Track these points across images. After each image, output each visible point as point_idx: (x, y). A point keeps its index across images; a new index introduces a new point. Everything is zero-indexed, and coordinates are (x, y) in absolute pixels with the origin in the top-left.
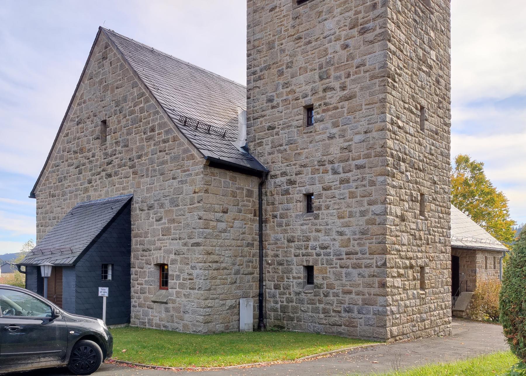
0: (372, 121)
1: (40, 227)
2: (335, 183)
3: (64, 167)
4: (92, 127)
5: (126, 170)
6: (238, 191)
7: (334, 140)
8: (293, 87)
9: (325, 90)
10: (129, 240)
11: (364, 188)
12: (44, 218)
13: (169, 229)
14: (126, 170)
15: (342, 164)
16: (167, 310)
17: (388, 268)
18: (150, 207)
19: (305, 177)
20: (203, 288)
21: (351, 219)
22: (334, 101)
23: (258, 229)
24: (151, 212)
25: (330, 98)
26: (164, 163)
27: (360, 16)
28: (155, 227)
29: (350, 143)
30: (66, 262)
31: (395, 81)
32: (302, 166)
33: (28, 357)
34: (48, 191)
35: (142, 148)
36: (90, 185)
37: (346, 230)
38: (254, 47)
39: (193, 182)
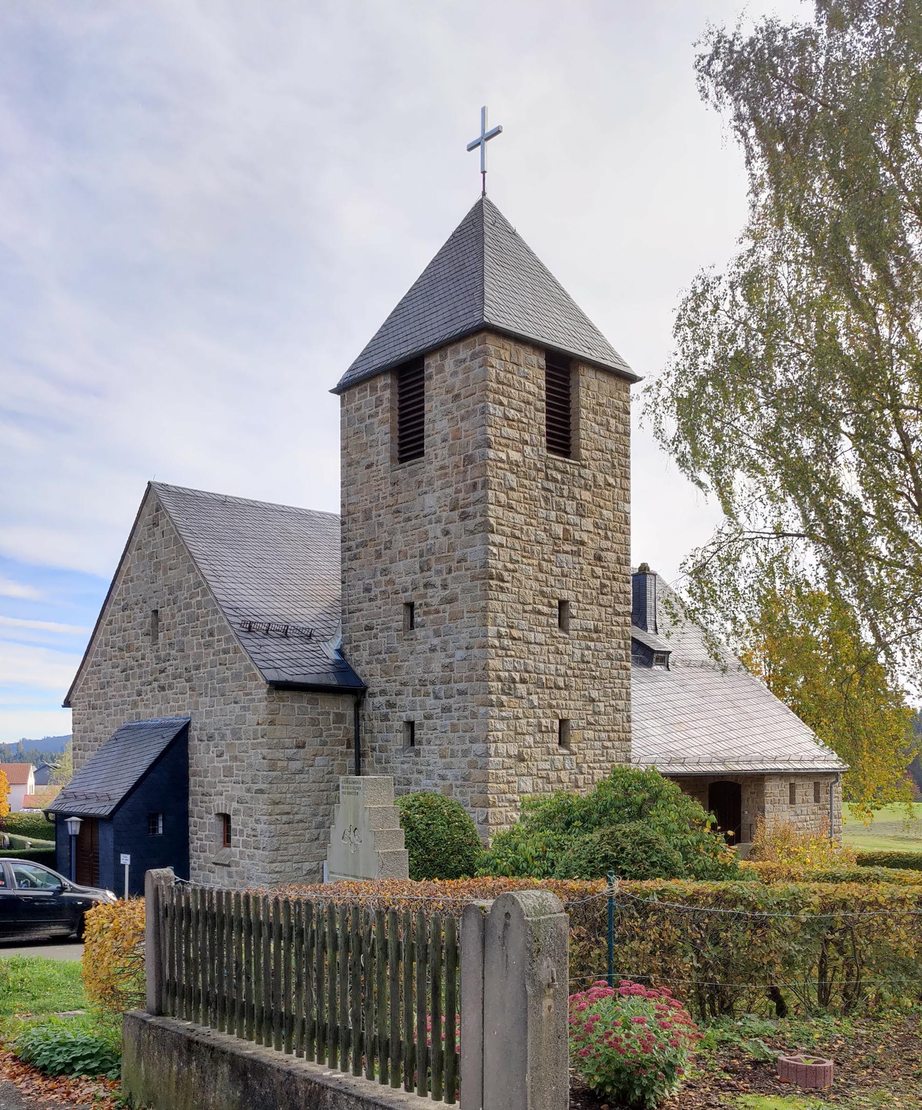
0: (474, 635)
1: (77, 751)
2: (436, 711)
3: (106, 668)
4: (140, 616)
5: (181, 684)
6: (321, 717)
7: (436, 653)
8: (392, 576)
9: (426, 586)
10: (187, 780)
11: (466, 721)
12: (82, 738)
13: (231, 768)
14: (181, 684)
15: (443, 687)
16: (230, 875)
17: (492, 825)
18: (211, 738)
19: (405, 700)
20: (268, 848)
21: (453, 760)
22: (435, 601)
23: (353, 765)
24: (211, 743)
25: (431, 597)
26: (224, 680)
27: (461, 495)
28: (215, 764)
29: (452, 660)
30: (102, 813)
31: (503, 581)
32: (402, 684)
33: (38, 925)
34: (86, 699)
35: (199, 656)
36: (139, 698)
37: (449, 773)
38: (349, 513)
39: (256, 709)
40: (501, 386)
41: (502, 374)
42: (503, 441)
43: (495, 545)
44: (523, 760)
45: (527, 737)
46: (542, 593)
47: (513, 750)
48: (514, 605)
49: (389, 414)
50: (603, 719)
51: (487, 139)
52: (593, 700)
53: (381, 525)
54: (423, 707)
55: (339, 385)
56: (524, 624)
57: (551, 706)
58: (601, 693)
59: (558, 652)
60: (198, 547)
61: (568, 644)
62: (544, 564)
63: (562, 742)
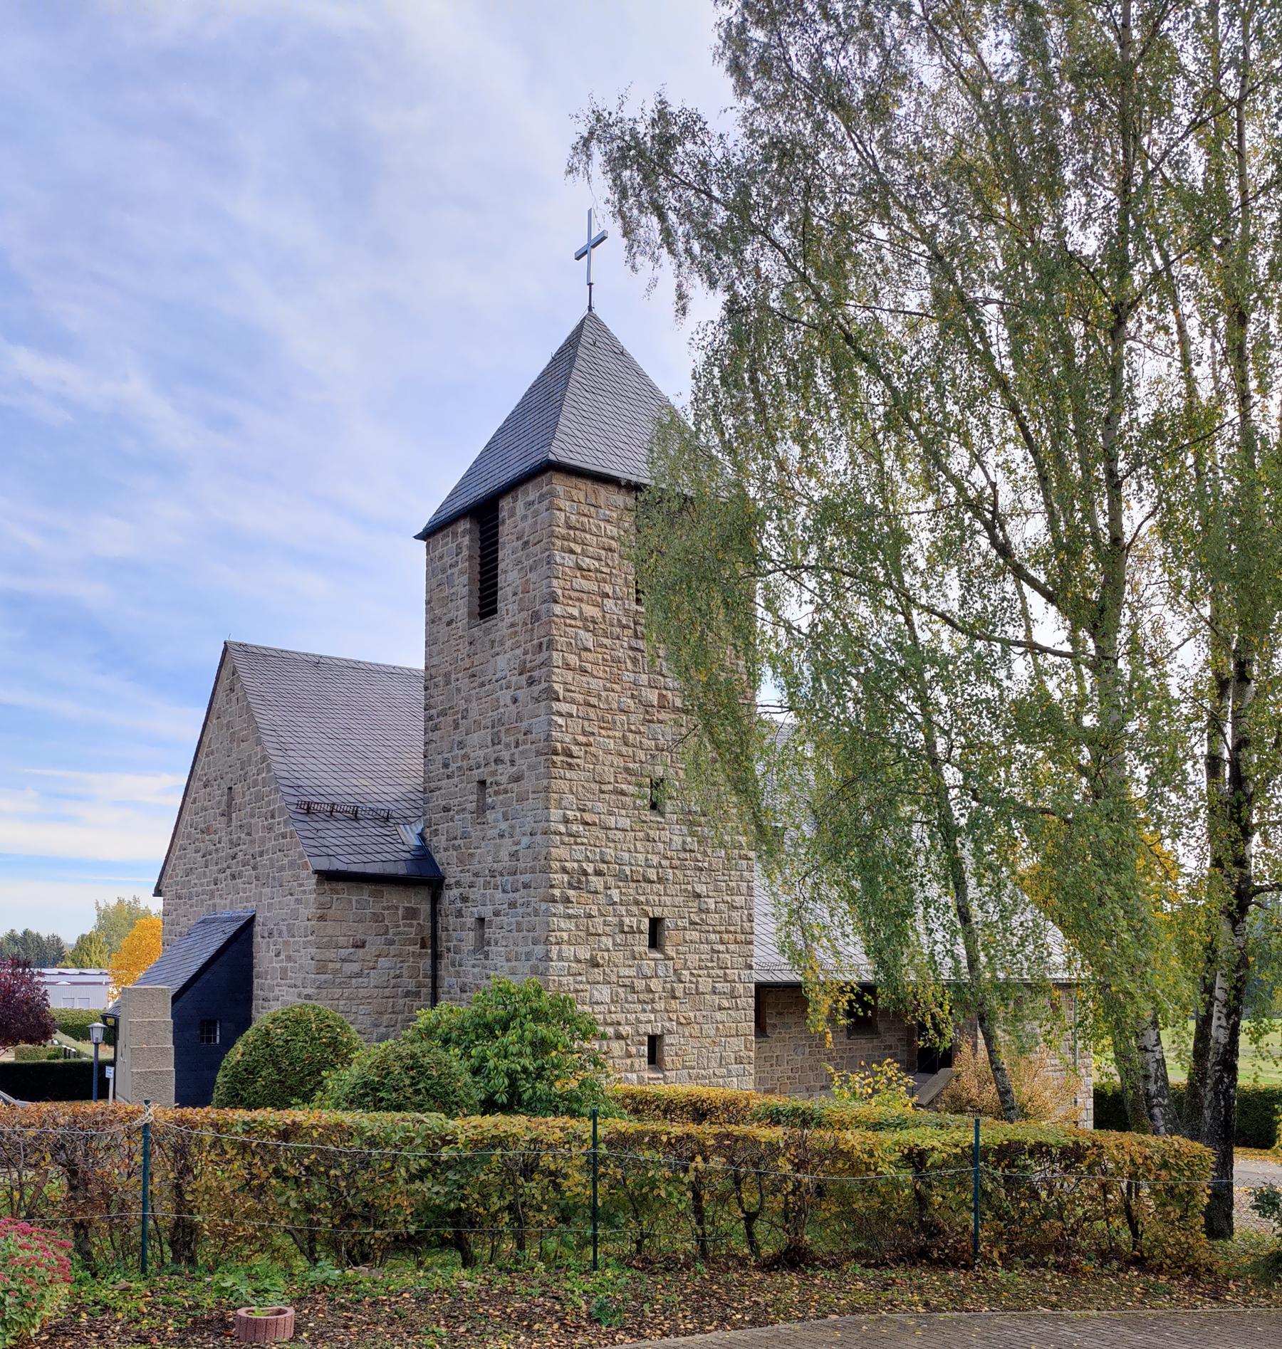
4: (218, 793)
14: (248, 872)
15: (510, 878)
26: (281, 869)
27: (529, 657)
31: (572, 756)
38: (432, 677)
40: (572, 532)
41: (573, 517)
42: (573, 594)
43: (561, 715)
44: (597, 965)
45: (604, 938)
46: (627, 770)
47: (584, 953)
48: (586, 784)
49: (467, 564)
50: (713, 918)
51: (594, 246)
52: (699, 896)
53: (458, 690)
54: (493, 903)
55: (425, 529)
56: (601, 807)
57: (637, 903)
58: (711, 887)
59: (648, 839)
60: (266, 717)
61: (663, 829)
62: (631, 736)
63: (655, 943)
